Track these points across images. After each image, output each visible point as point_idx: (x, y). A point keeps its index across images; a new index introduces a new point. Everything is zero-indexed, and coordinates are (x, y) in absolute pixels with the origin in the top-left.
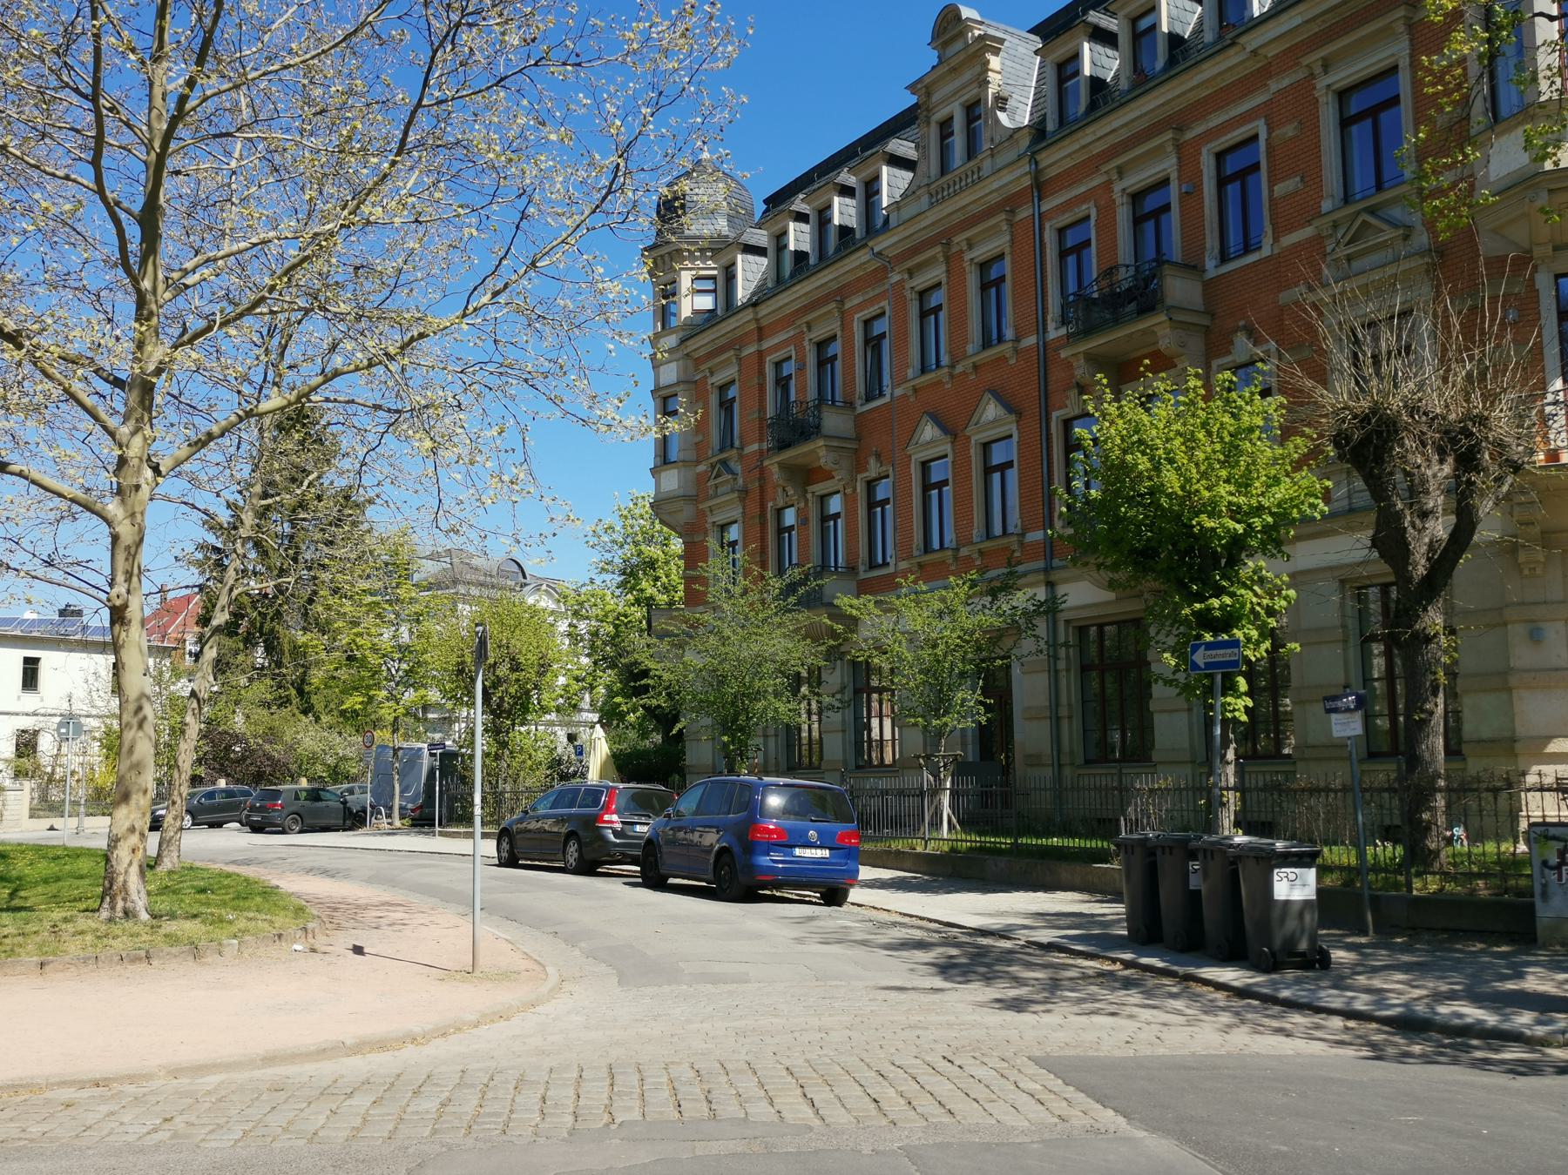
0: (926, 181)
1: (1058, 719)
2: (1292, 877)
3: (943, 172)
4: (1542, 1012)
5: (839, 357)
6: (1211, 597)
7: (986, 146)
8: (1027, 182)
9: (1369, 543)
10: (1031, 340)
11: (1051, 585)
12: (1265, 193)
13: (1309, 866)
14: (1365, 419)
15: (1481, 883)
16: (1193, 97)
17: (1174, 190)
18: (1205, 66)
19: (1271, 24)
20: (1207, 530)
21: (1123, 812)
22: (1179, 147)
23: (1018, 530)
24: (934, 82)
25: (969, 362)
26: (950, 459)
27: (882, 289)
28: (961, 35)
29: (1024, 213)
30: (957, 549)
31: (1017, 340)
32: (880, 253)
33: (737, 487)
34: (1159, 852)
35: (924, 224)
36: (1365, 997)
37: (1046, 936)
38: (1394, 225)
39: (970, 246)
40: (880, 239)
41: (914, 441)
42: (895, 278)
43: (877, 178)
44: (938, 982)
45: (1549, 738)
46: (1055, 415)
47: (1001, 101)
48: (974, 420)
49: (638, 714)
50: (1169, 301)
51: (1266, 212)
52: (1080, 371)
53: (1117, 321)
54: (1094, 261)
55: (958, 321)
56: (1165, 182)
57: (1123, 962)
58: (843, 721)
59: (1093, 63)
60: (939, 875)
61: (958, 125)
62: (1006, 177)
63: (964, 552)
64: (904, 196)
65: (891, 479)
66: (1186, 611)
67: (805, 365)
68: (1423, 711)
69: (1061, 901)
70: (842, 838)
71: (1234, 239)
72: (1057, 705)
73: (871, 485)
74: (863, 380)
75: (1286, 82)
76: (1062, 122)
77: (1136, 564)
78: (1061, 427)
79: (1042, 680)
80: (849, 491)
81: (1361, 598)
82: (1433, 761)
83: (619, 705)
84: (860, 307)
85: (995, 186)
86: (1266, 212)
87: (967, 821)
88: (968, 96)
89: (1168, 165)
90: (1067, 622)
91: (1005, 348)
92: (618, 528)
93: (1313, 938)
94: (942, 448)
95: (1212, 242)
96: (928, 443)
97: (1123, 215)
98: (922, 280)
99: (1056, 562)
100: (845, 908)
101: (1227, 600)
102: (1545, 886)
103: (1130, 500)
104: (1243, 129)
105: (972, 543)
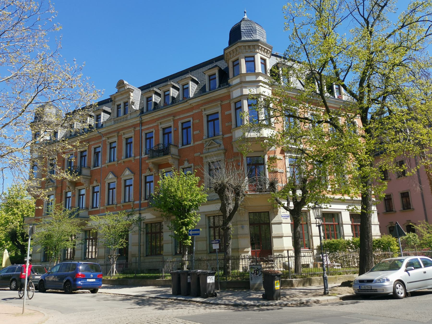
0: (113, 118)
2: (211, 278)
3: (118, 116)
5: (87, 156)
7: (129, 112)
8: (139, 122)
9: (219, 209)
10: (138, 157)
13: (213, 275)
14: (220, 185)
15: (239, 278)
17: (172, 128)
21: (163, 267)
24: (116, 96)
26: (116, 183)
27: (100, 141)
30: (117, 204)
31: (135, 157)
32: (100, 133)
34: (181, 275)
35: (112, 128)
37: (154, 295)
38: (218, 143)
39: (124, 134)
40: (101, 129)
41: (107, 178)
42: (104, 139)
43: (100, 115)
45: (245, 248)
46: (143, 175)
47: (133, 103)
48: (123, 174)
50: (172, 153)
52: (151, 166)
53: (159, 156)
54: (154, 142)
55: (120, 151)
56: (171, 127)
57: (174, 299)
58: (82, 247)
59: (155, 99)
60: (115, 285)
61: (122, 106)
62: (134, 120)
64: (107, 120)
65: (99, 187)
68: (228, 243)
69: (150, 288)
71: (185, 141)
72: (140, 242)
73: (93, 188)
75: (197, 111)
79: (137, 236)
80: (88, 189)
81: (209, 217)
84: (94, 144)
85: (131, 122)
87: (120, 271)
88: (126, 100)
89: (171, 124)
90: (144, 222)
91: (132, 159)
92: (7, 194)
93: (214, 291)
95: (180, 141)
96: (111, 179)
97: (161, 133)
98: (111, 140)
100: (97, 293)
101: (188, 219)
102: (251, 277)
103: (169, 197)
105: (121, 203)
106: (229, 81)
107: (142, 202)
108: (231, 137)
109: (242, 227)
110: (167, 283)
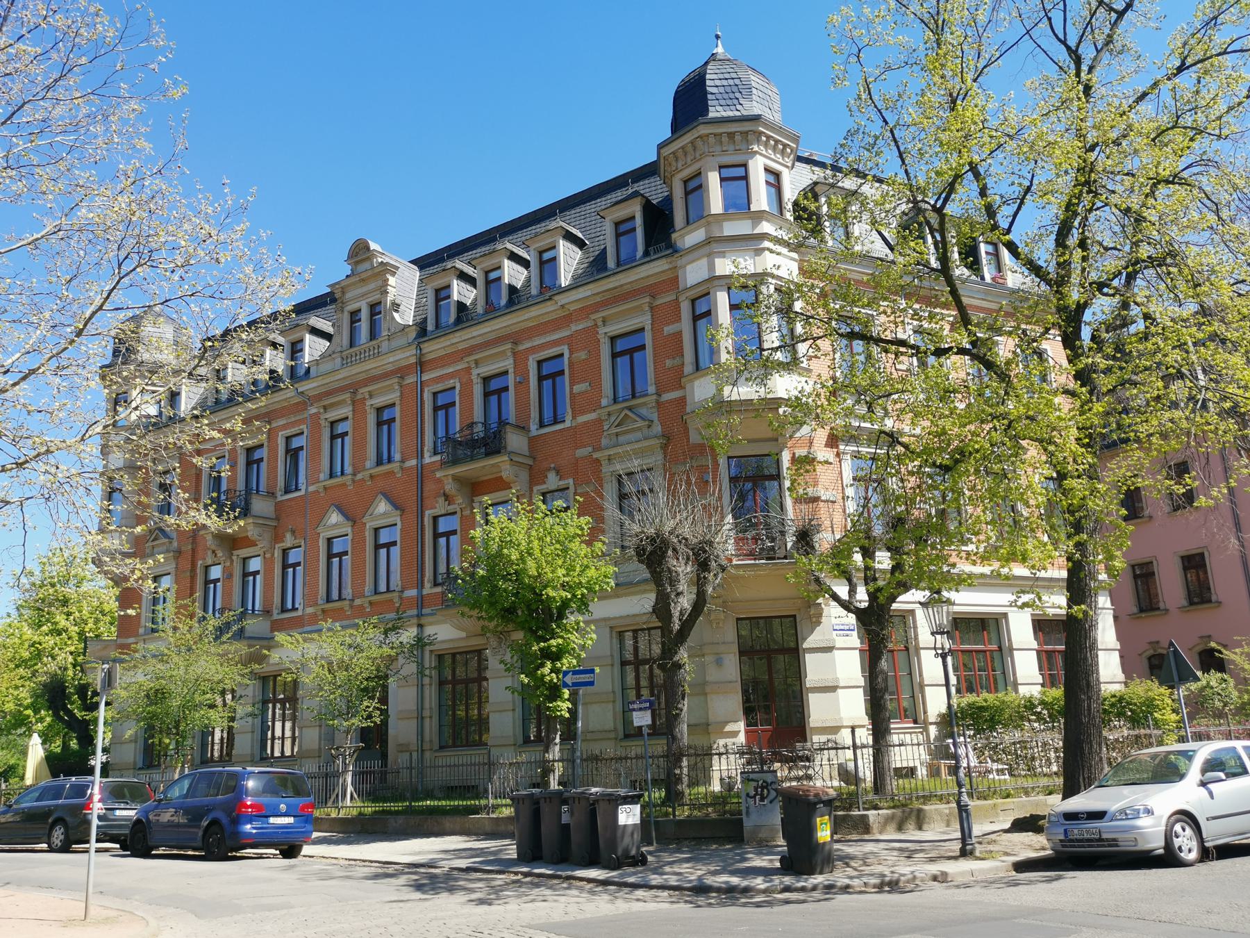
1: (422, 718)
2: (628, 810)
3: (352, 345)
4: (765, 876)
5: (265, 460)
6: (551, 638)
8: (413, 360)
10: (413, 462)
11: (420, 626)
12: (567, 389)
15: (710, 809)
16: (524, 325)
17: (511, 377)
18: (532, 309)
19: (574, 292)
20: (551, 598)
22: (514, 354)
23: (399, 589)
24: (348, 286)
25: (367, 473)
26: (349, 537)
28: (369, 259)
29: (411, 379)
30: (353, 600)
31: (403, 461)
32: (302, 393)
33: (172, 548)
34: (542, 801)
36: (675, 877)
38: (643, 419)
39: (371, 396)
41: (322, 524)
44: (418, 895)
45: (727, 723)
46: (427, 513)
47: (396, 306)
49: (45, 724)
50: (509, 448)
51: (568, 400)
52: (450, 487)
53: (472, 458)
55: (360, 445)
57: (522, 873)
58: (253, 724)
61: (365, 315)
62: (400, 355)
63: (358, 602)
64: (323, 356)
65: (302, 549)
66: (535, 648)
67: (236, 463)
68: (677, 709)
69: (451, 842)
70: (303, 809)
71: (548, 414)
72: (422, 709)
73: (285, 552)
74: (283, 478)
75: (580, 327)
76: (437, 326)
77: (503, 617)
78: (431, 521)
79: (412, 692)
80: (268, 556)
82: (682, 738)
83: (29, 716)
84: (284, 427)
85: (391, 360)
86: (568, 400)
89: (508, 363)
91: (394, 466)
94: (345, 529)
95: (534, 414)
97: (478, 390)
98: (334, 415)
99: (425, 611)
100: (300, 858)
103: (504, 577)
104: (554, 349)
105: (364, 596)
106: (674, 236)
107: (425, 592)
108: (682, 401)
109: (719, 663)
110: (502, 828)
